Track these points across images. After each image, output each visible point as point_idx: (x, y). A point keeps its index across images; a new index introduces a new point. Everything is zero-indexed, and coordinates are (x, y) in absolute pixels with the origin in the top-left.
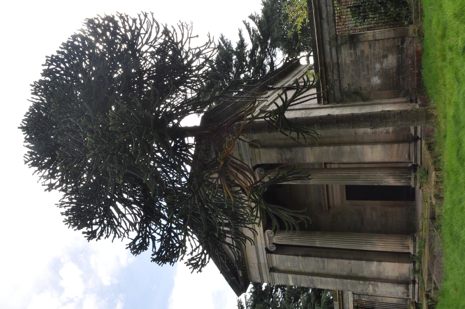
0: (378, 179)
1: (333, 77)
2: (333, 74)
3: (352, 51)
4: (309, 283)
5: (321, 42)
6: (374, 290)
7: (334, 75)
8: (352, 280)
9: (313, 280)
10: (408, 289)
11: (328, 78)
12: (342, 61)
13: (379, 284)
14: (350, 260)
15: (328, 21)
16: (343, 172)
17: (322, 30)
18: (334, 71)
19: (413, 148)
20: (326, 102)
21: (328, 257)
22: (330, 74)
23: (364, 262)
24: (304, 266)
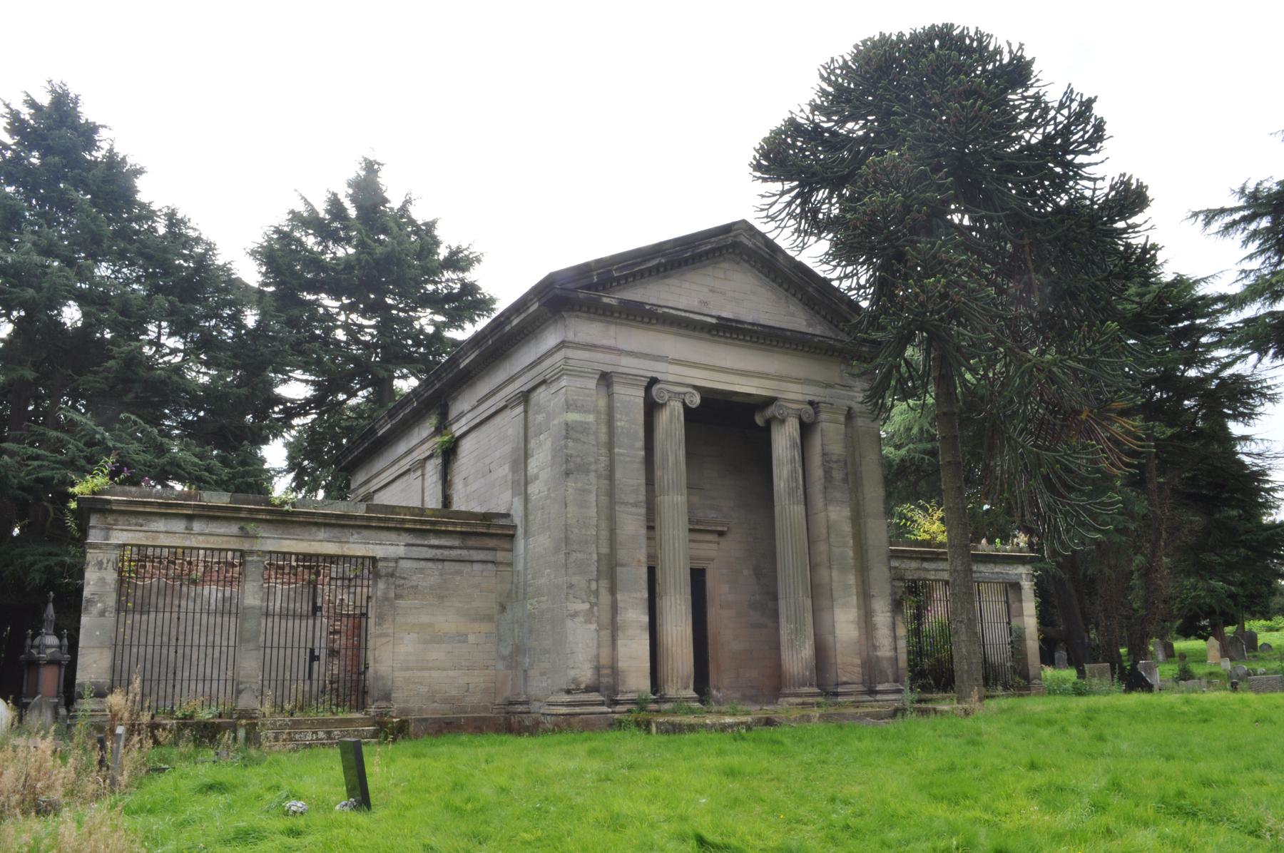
4: (578, 460)
10: (589, 689)
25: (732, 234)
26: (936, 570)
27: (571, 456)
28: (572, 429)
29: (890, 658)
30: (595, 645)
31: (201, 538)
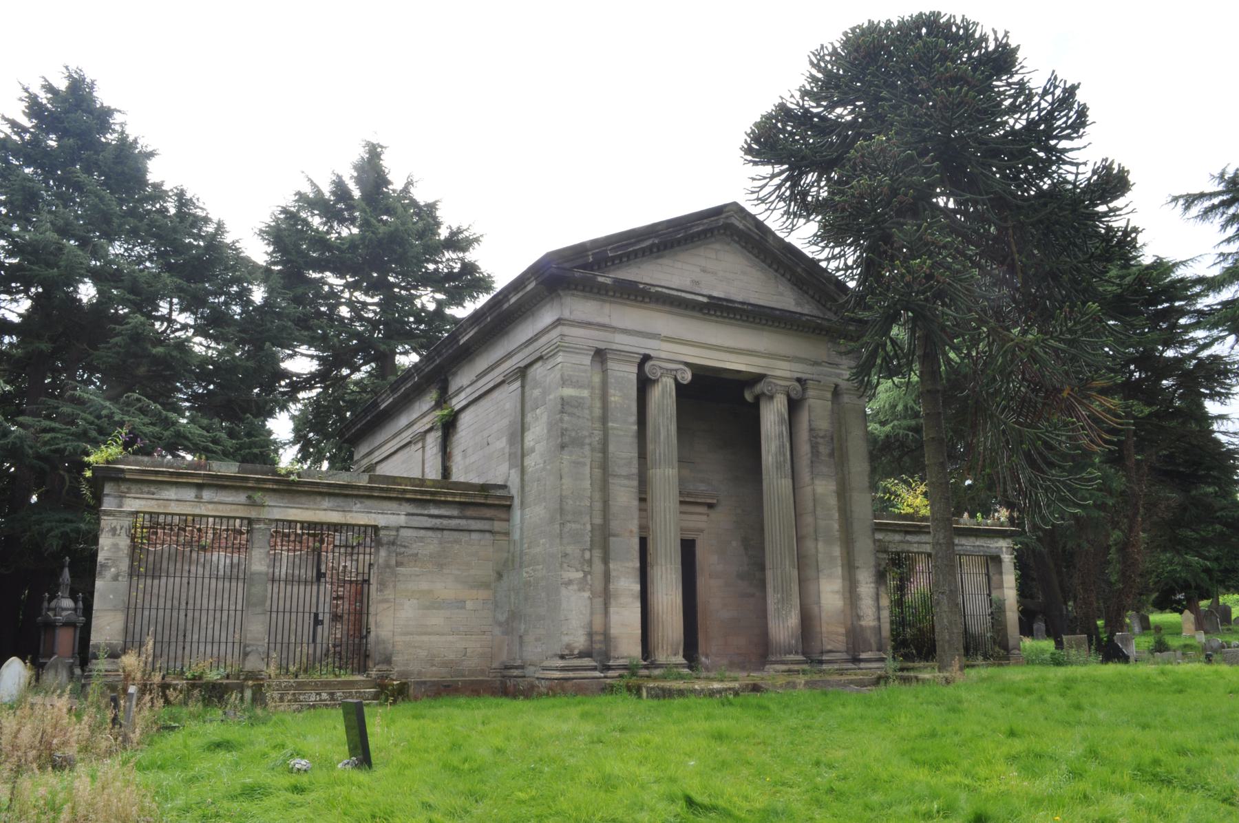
4: (573, 434)
10: (582, 655)
15: (902, 542)
25: (723, 216)
26: (919, 543)
27: (566, 430)
28: (568, 403)
30: (589, 611)
31: (210, 506)
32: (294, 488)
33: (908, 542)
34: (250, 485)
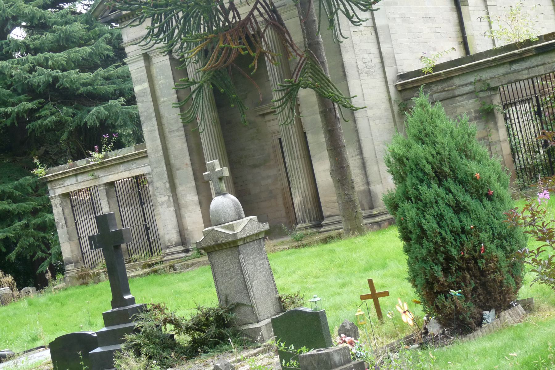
0: (296, 183)
1: (435, 93)
2: (439, 92)
3: (473, 115)
4: (145, 114)
5: (477, 69)
6: (162, 204)
7: (439, 94)
8: (166, 172)
9: (151, 119)
10: (176, 245)
11: (433, 86)
12: (459, 102)
13: (172, 209)
14: (190, 165)
15: (508, 73)
16: (296, 137)
17: (495, 66)
18: (443, 93)
19: (338, 220)
20: (400, 88)
21: (186, 135)
22: (440, 87)
23: (194, 184)
24: (166, 103)
26: (528, 68)
29: (364, 191)
31: (82, 184)
32: (104, 165)
33: (515, 71)
34: (88, 170)
